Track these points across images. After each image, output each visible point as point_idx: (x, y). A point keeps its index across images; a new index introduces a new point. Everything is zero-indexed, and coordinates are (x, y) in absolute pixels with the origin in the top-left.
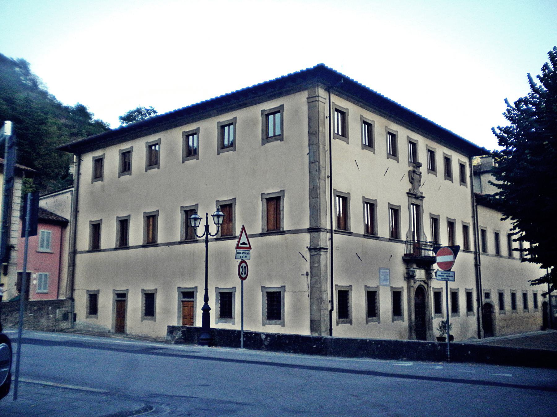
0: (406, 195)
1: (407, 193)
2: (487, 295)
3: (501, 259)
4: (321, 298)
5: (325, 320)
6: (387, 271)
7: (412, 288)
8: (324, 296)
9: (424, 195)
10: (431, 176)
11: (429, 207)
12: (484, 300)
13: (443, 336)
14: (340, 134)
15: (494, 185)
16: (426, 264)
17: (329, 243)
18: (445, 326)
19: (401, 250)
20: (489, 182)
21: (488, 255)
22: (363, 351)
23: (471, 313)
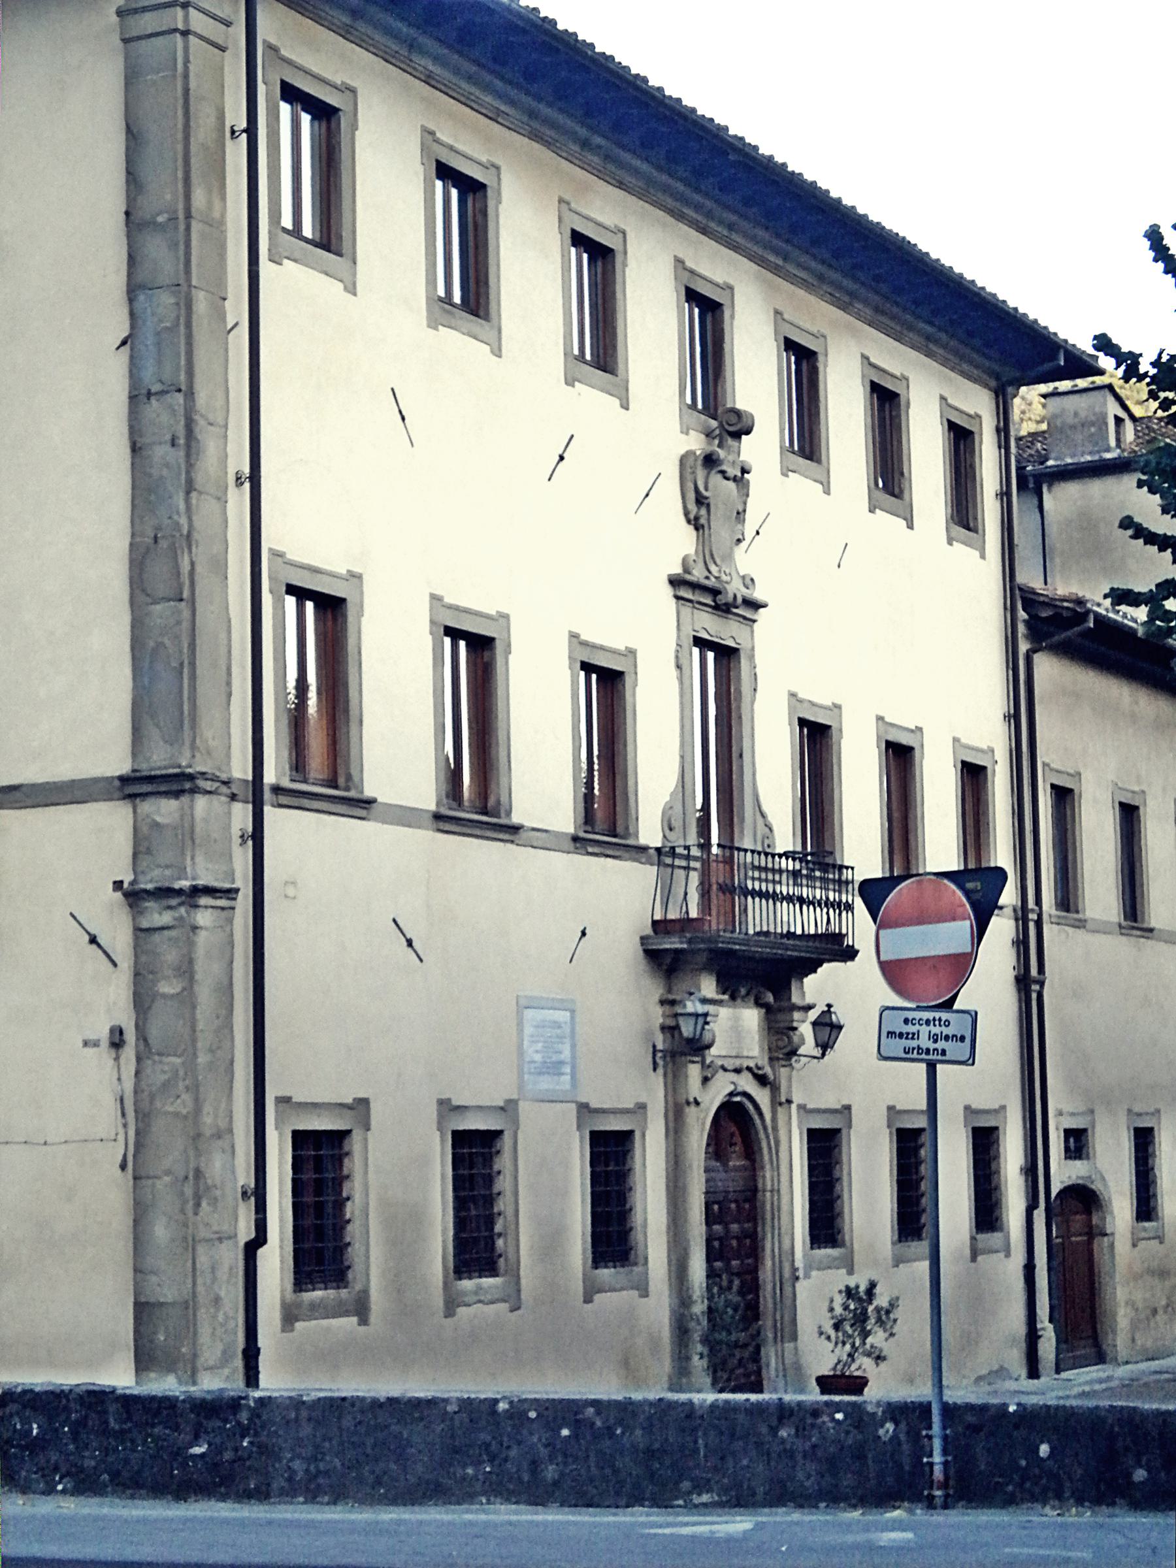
0: (668, 591)
1: (675, 582)
2: (1078, 1143)
3: (1150, 946)
4: (198, 1173)
5: (217, 1300)
6: (563, 1016)
7: (691, 1111)
8: (215, 1166)
9: (758, 595)
10: (801, 486)
11: (784, 671)
12: (1063, 1172)
13: (853, 1370)
14: (307, 231)
15: (1151, 538)
16: (769, 974)
17: (242, 859)
18: (860, 1313)
19: (624, 897)
20: (1127, 523)
21: (1081, 924)
22: (477, 1463)
23: (994, 1239)
